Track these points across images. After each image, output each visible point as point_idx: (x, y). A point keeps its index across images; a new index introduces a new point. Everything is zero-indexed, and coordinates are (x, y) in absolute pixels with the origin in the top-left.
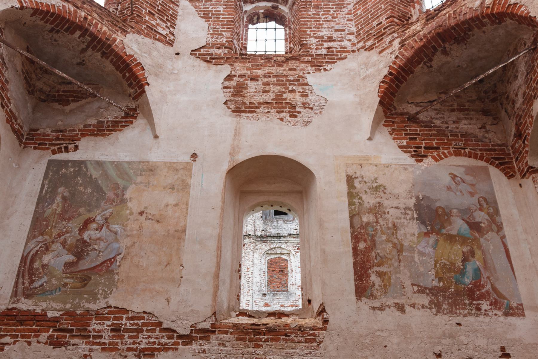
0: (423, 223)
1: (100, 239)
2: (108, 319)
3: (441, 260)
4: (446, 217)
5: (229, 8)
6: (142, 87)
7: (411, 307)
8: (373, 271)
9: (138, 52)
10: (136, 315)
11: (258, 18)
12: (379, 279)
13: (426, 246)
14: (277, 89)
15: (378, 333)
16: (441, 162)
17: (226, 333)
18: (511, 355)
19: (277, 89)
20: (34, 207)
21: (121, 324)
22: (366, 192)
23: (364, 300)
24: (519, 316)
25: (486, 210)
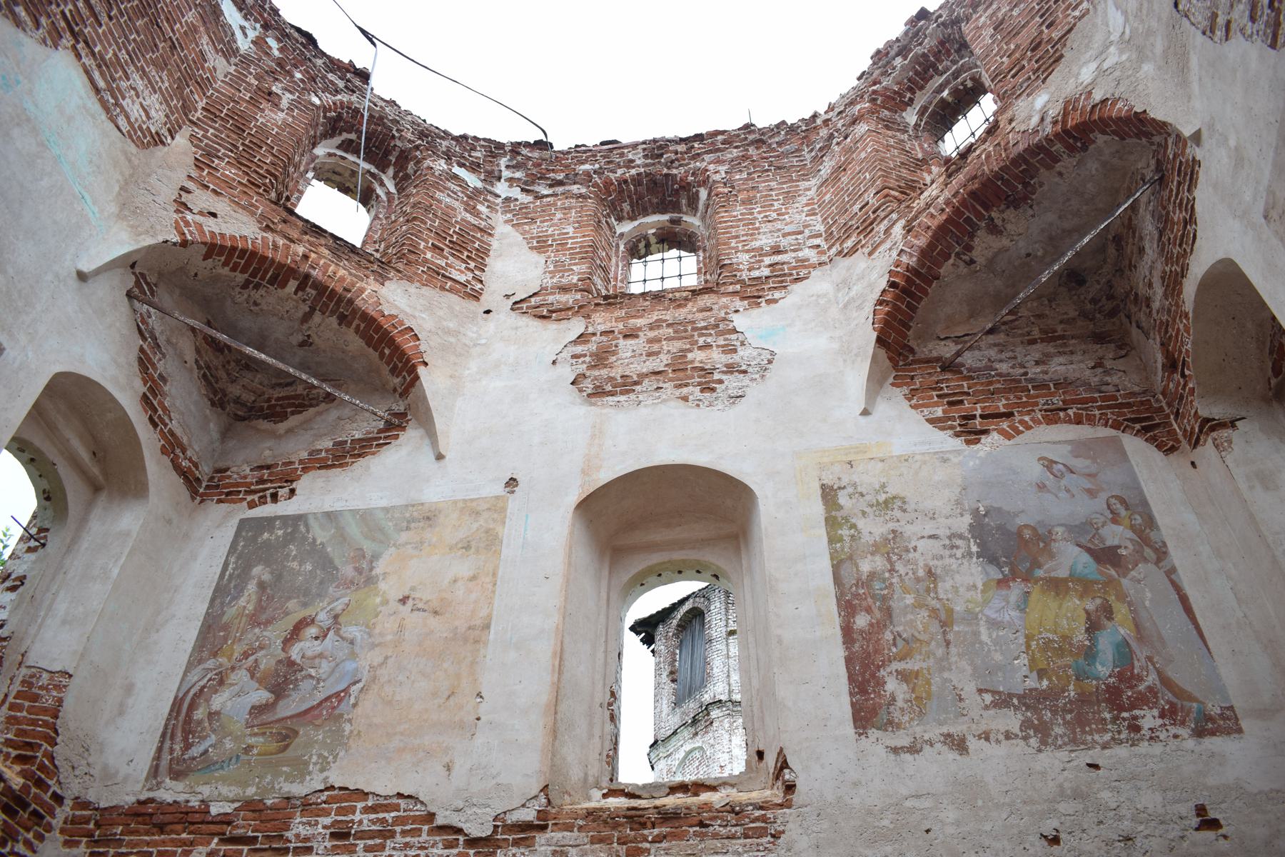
0: (993, 560)
1: (321, 656)
2: (327, 813)
3: (1040, 633)
4: (1042, 545)
5: (585, 226)
6: (412, 370)
7: (980, 738)
8: (889, 670)
9: (408, 310)
10: (382, 801)
11: (648, 246)
12: (905, 686)
13: (1004, 607)
14: (676, 346)
15: (908, 804)
16: (1018, 439)
17: (569, 828)
18: (1222, 822)
19: (676, 346)
20: (206, 605)
21: (352, 821)
22: (864, 513)
23: (874, 733)
24: (1229, 734)
25: (1127, 522)
